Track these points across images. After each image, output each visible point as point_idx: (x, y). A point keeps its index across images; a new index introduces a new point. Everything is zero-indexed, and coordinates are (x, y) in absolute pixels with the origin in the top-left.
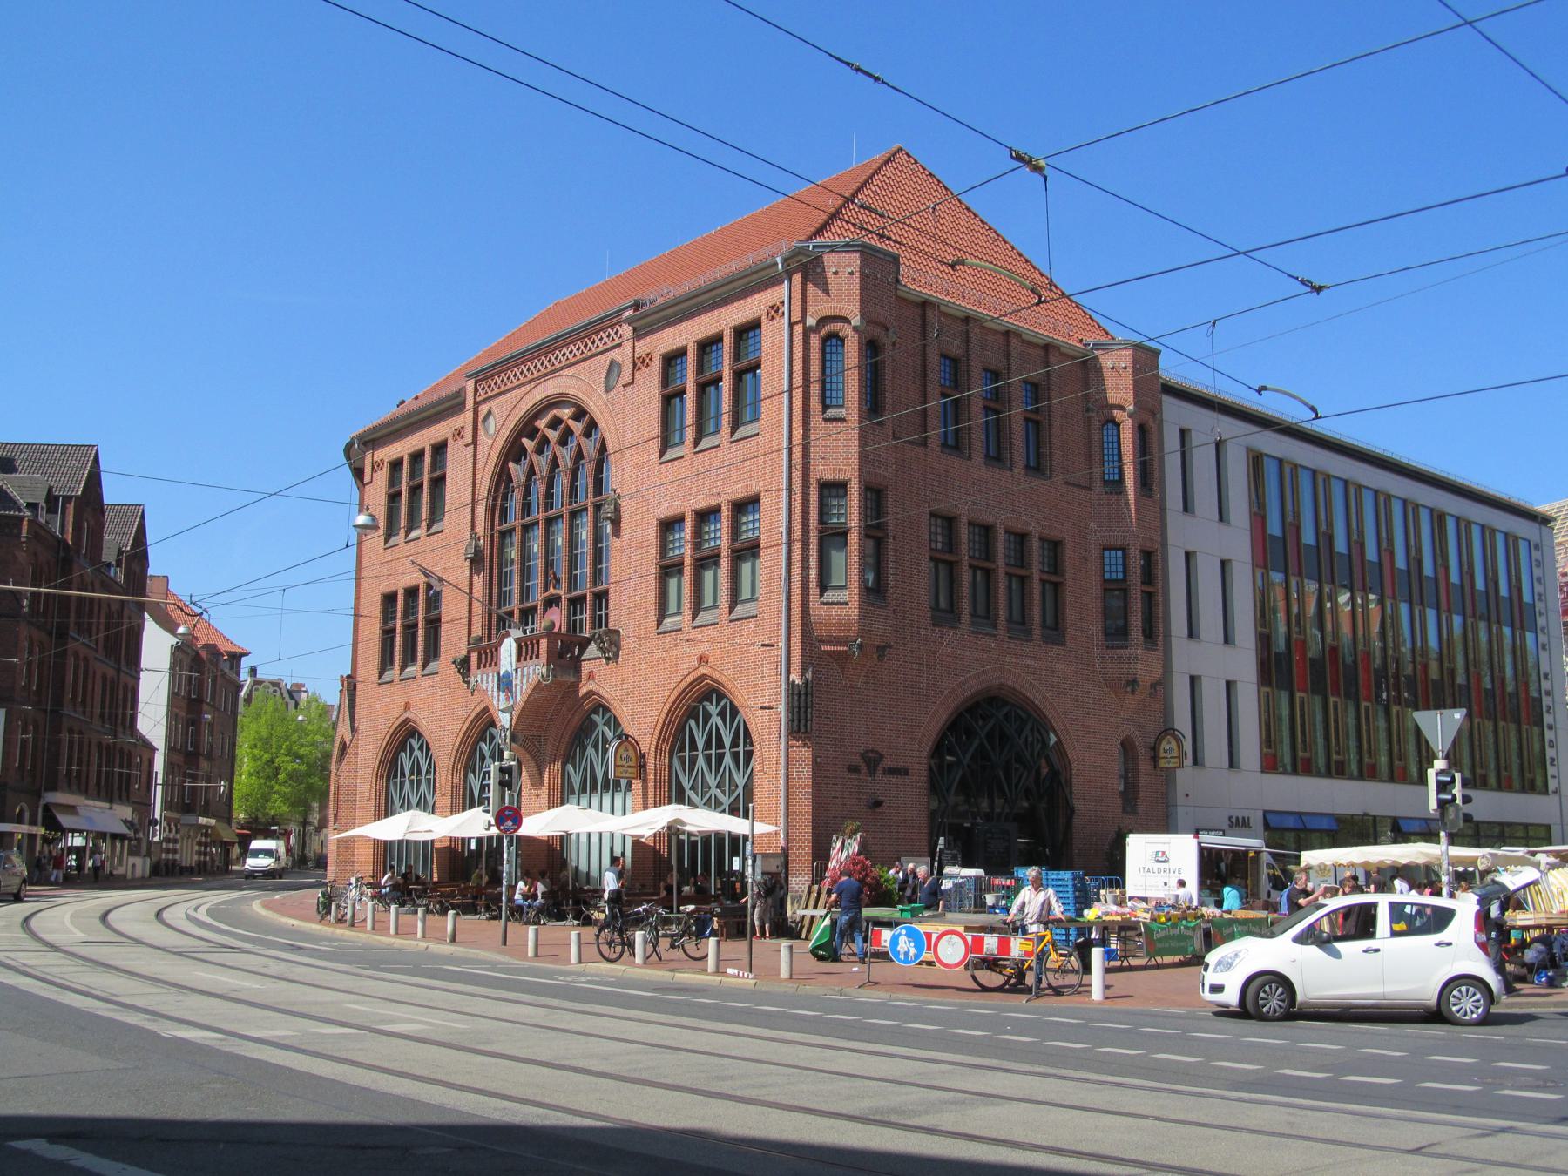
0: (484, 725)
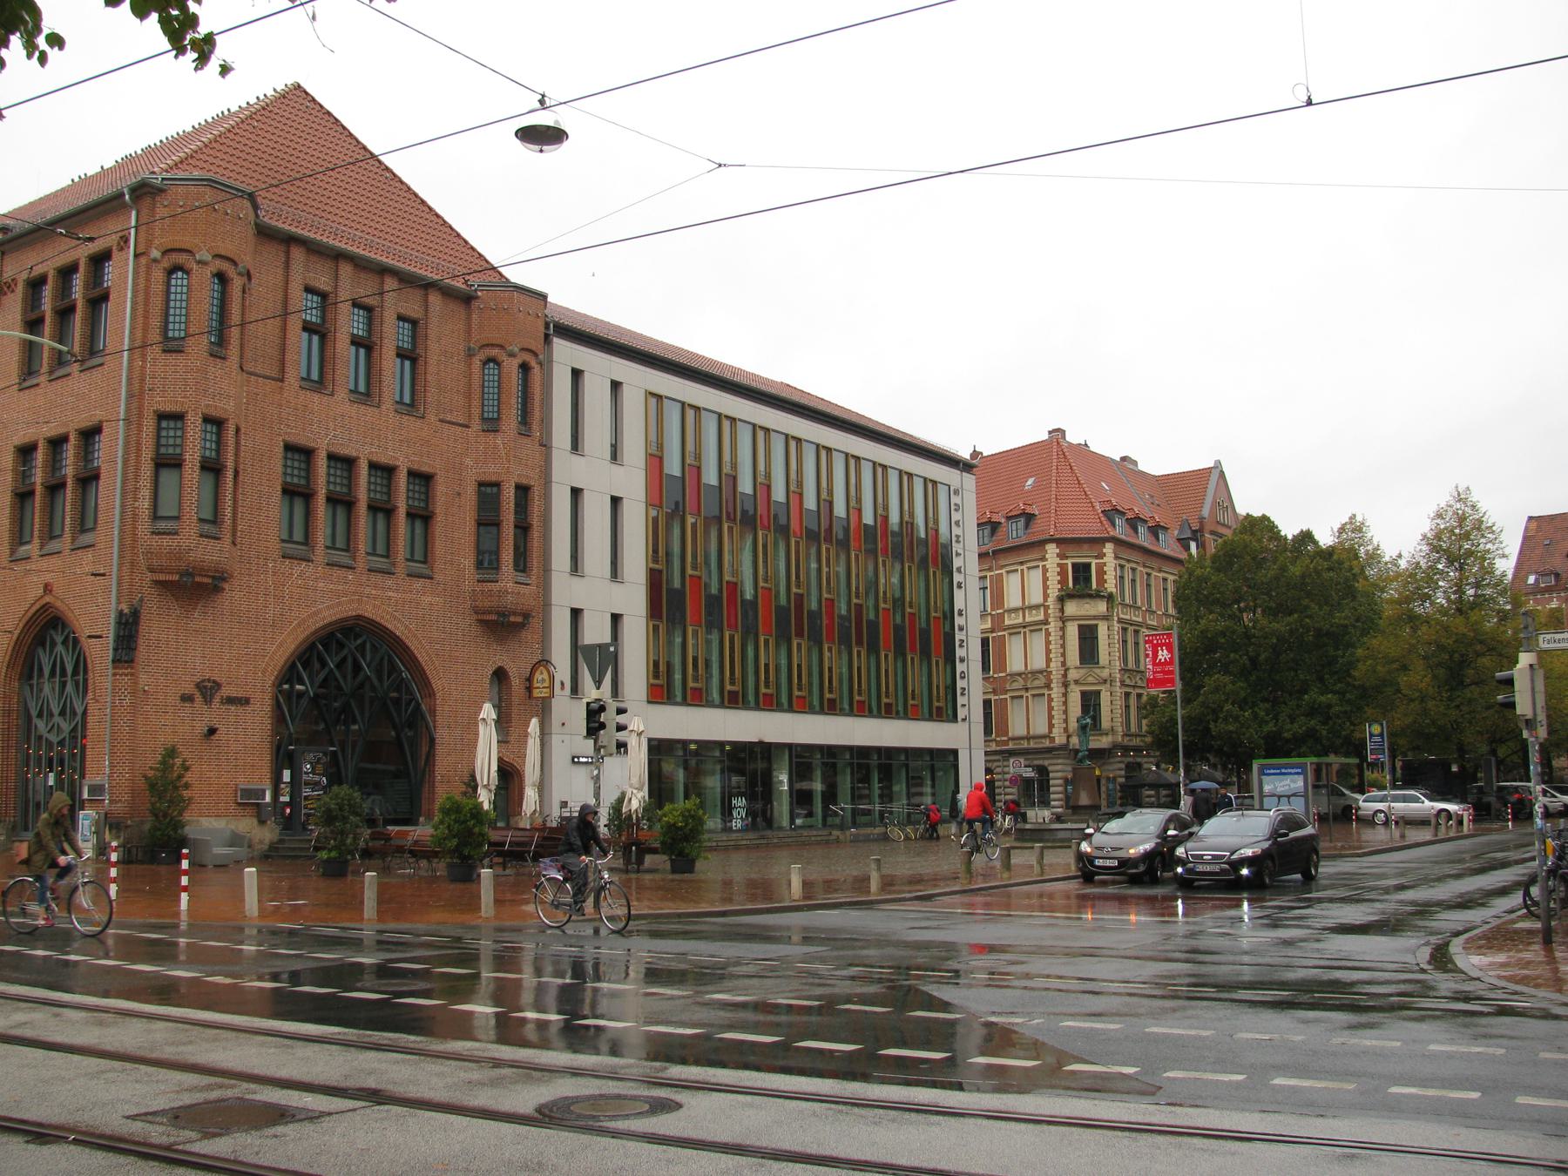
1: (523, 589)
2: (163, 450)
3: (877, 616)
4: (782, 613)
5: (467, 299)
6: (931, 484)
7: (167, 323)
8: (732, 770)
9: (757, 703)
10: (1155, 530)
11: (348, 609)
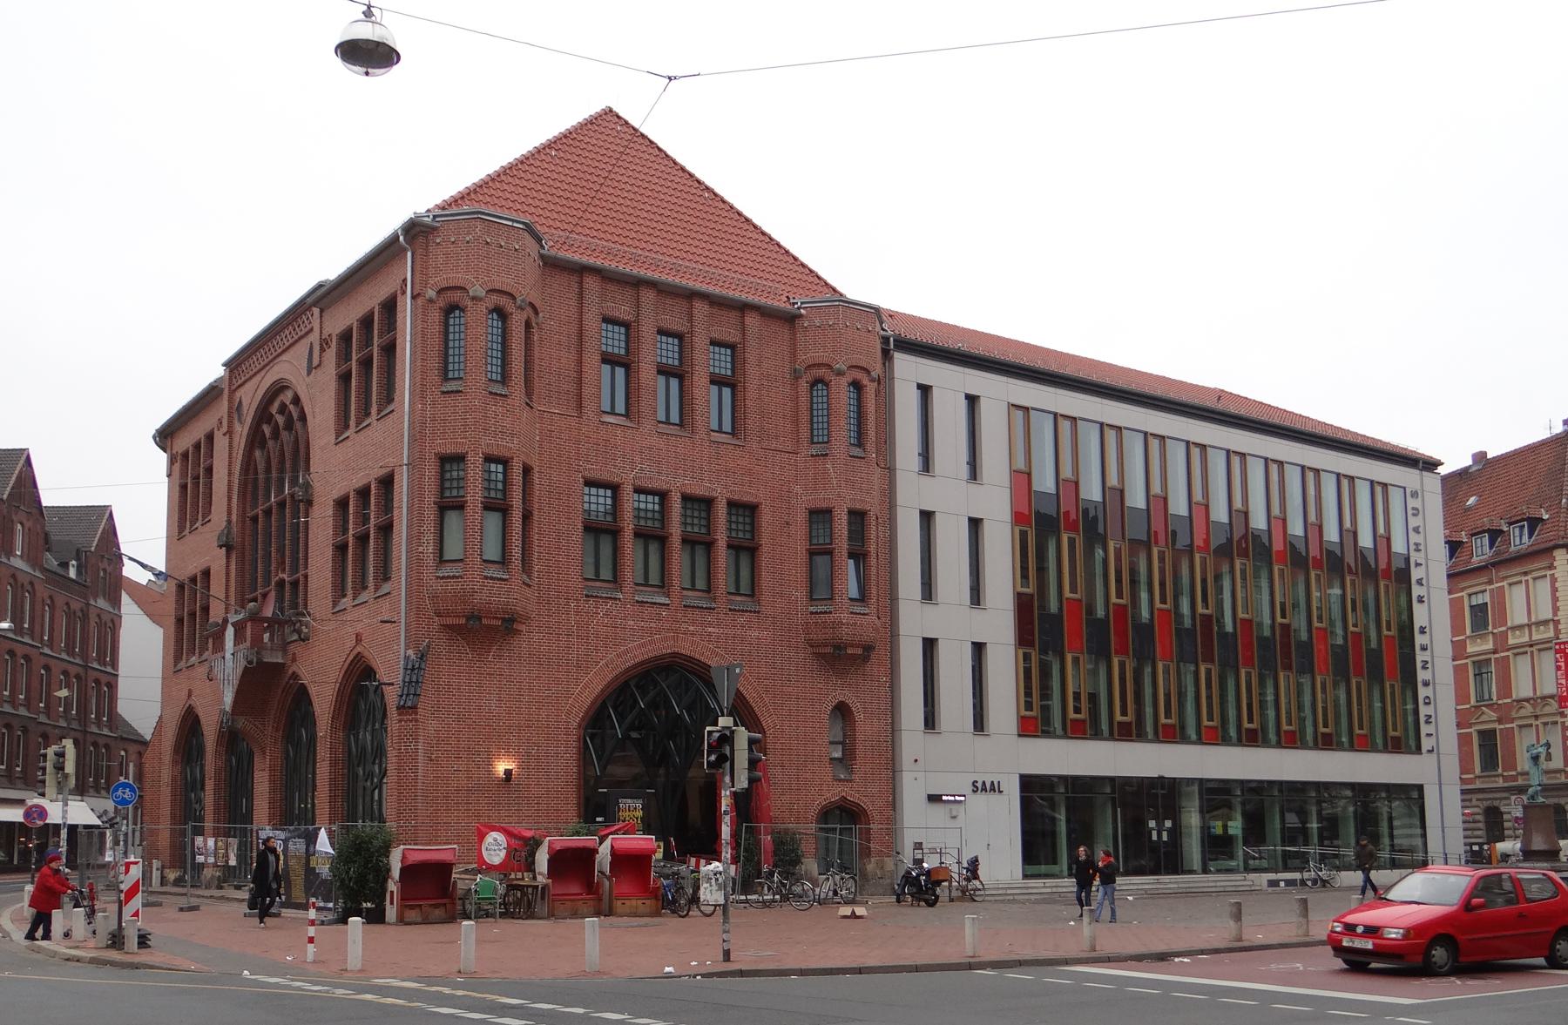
1: (859, 620)
2: (447, 494)
3: (1310, 638)
4: (1266, 644)
5: (790, 319)
6: (1379, 488)
7: (446, 363)
8: (611, 818)
9: (1156, 733)
11: (665, 648)
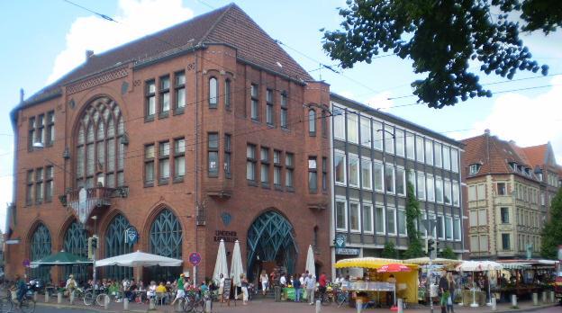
0: (73, 220)
10: (527, 170)
